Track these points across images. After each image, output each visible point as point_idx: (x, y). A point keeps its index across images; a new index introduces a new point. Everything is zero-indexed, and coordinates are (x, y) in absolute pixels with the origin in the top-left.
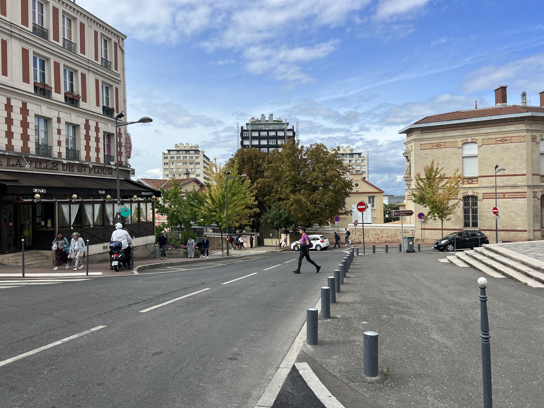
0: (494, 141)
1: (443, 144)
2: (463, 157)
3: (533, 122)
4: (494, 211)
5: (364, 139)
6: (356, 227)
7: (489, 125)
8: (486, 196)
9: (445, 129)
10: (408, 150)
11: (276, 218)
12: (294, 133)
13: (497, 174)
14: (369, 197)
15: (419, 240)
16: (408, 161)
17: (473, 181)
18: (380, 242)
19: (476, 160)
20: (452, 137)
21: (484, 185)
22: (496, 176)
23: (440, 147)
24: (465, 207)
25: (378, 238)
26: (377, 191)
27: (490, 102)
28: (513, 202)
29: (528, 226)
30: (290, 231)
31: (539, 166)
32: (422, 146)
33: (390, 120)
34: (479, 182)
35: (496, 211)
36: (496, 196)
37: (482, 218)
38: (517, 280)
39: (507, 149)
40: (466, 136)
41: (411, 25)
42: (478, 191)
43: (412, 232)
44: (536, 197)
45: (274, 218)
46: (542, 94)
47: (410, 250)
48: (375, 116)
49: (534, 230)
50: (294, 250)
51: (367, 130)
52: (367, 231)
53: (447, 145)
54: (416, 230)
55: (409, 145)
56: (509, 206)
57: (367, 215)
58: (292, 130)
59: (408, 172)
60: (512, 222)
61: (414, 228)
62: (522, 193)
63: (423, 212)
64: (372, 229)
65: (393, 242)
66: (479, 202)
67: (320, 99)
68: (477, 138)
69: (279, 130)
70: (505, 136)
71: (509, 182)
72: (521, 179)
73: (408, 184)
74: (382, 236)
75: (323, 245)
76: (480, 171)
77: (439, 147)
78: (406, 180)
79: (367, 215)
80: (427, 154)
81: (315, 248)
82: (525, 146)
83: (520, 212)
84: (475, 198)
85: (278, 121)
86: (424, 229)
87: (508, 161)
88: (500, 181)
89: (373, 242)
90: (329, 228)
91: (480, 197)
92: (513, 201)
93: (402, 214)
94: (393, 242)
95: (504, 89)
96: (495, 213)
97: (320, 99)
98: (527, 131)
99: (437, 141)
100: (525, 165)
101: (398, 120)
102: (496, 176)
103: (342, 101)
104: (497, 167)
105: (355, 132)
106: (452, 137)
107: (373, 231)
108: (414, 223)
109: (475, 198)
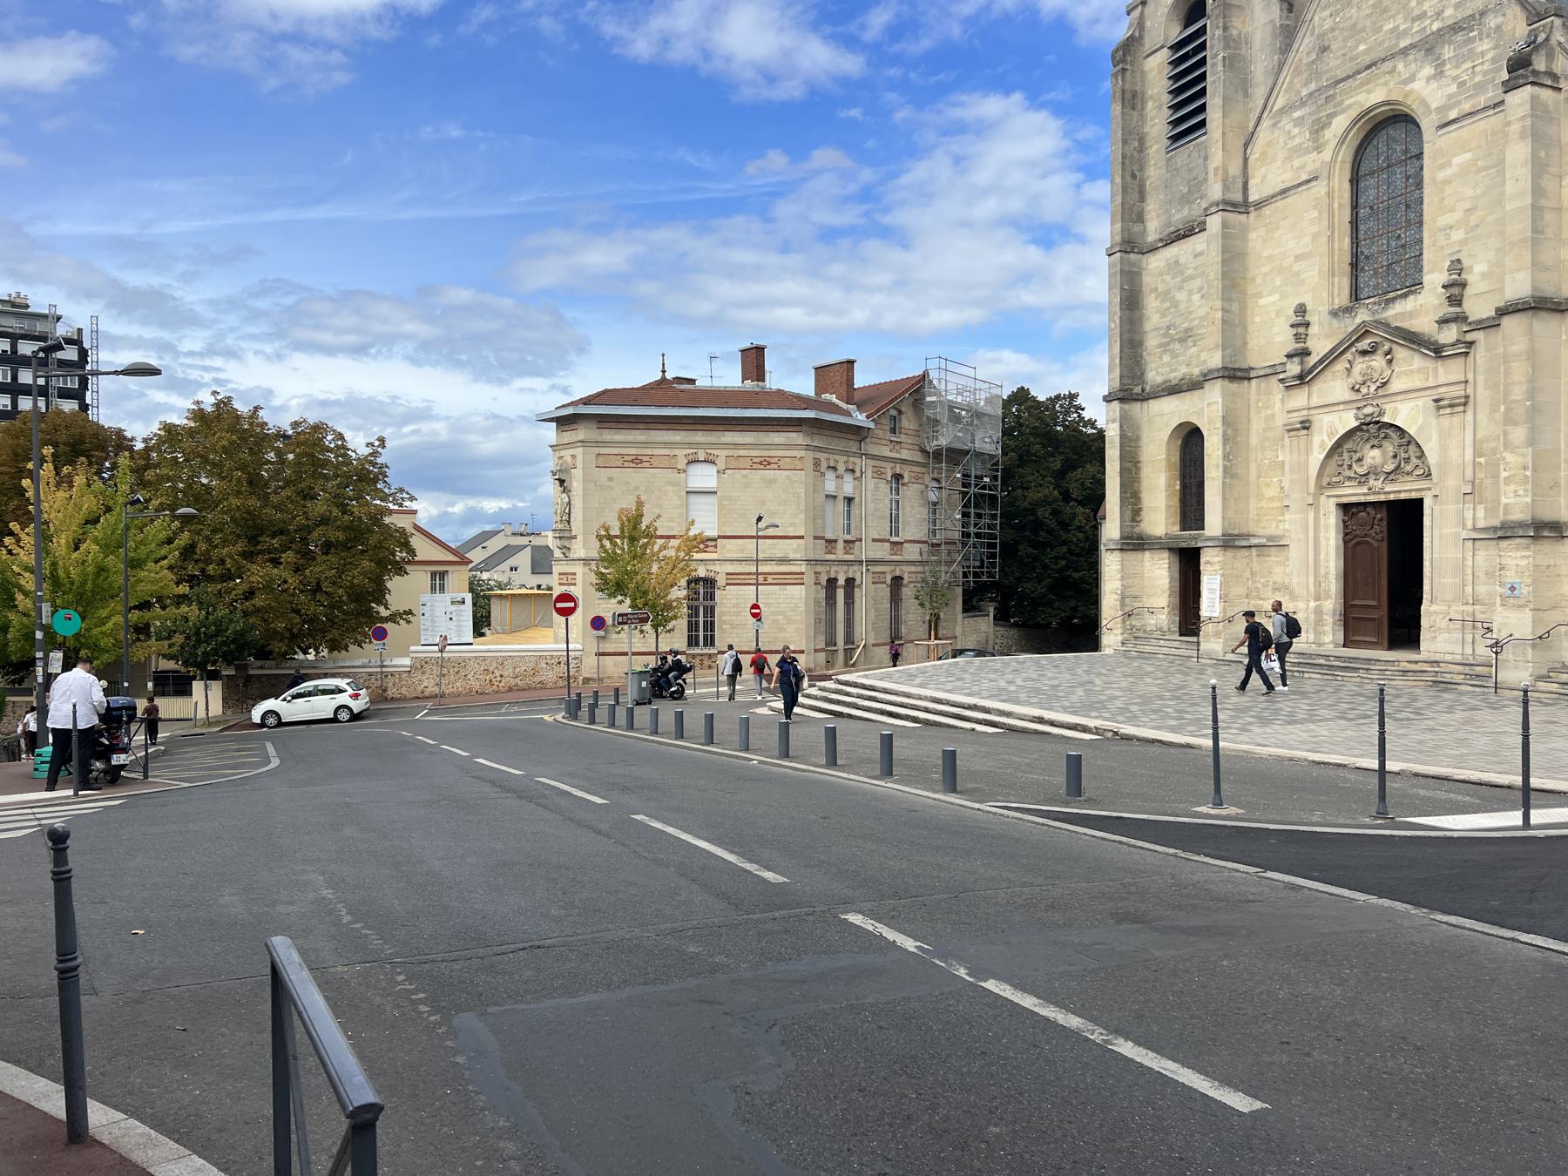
0: (748, 463)
1: (647, 458)
2: (687, 492)
3: (815, 430)
4: (753, 611)
5: (228, 381)
6: (444, 655)
7: (738, 428)
8: (734, 580)
9: (652, 426)
10: (565, 465)
11: (205, 633)
12: (83, 354)
13: (759, 534)
14: (434, 574)
16: (566, 490)
17: (707, 546)
18: (496, 689)
19: (712, 499)
20: (666, 444)
21: (729, 556)
22: (758, 537)
23: (640, 465)
24: (711, 603)
25: (491, 681)
27: (731, 377)
28: (780, 592)
29: (807, 642)
30: (224, 673)
31: (824, 520)
32: (601, 459)
33: (301, 334)
34: (718, 549)
35: (758, 611)
36: (759, 579)
37: (724, 626)
38: (956, 727)
39: (772, 482)
40: (694, 446)
41: (336, 57)
42: (717, 568)
44: (819, 584)
45: (197, 633)
46: (819, 370)
48: (255, 316)
49: (816, 651)
50: (262, 725)
51: (230, 354)
53: (655, 462)
55: (567, 453)
56: (773, 601)
57: (462, 623)
58: (76, 342)
59: (564, 518)
60: (779, 635)
62: (797, 574)
64: (476, 658)
65: (530, 689)
66: (718, 593)
67: (64, 228)
68: (716, 452)
69: (25, 337)
70: (766, 453)
71: (774, 552)
72: (795, 546)
74: (501, 676)
75: (357, 706)
76: (721, 524)
77: (637, 464)
79: (462, 623)
80: (611, 479)
82: (803, 479)
83: (793, 613)
84: (710, 583)
85: (14, 305)
86: (604, 654)
87: (773, 508)
88: (768, 548)
90: (362, 656)
91: (721, 581)
92: (781, 590)
94: (530, 689)
95: (760, 350)
96: (754, 615)
97: (64, 228)
98: (808, 447)
99: (633, 451)
100: (802, 516)
101: (326, 338)
102: (758, 537)
103: (142, 250)
104: (760, 519)
105: (191, 354)
106: (666, 444)
108: (581, 641)
109: (710, 583)
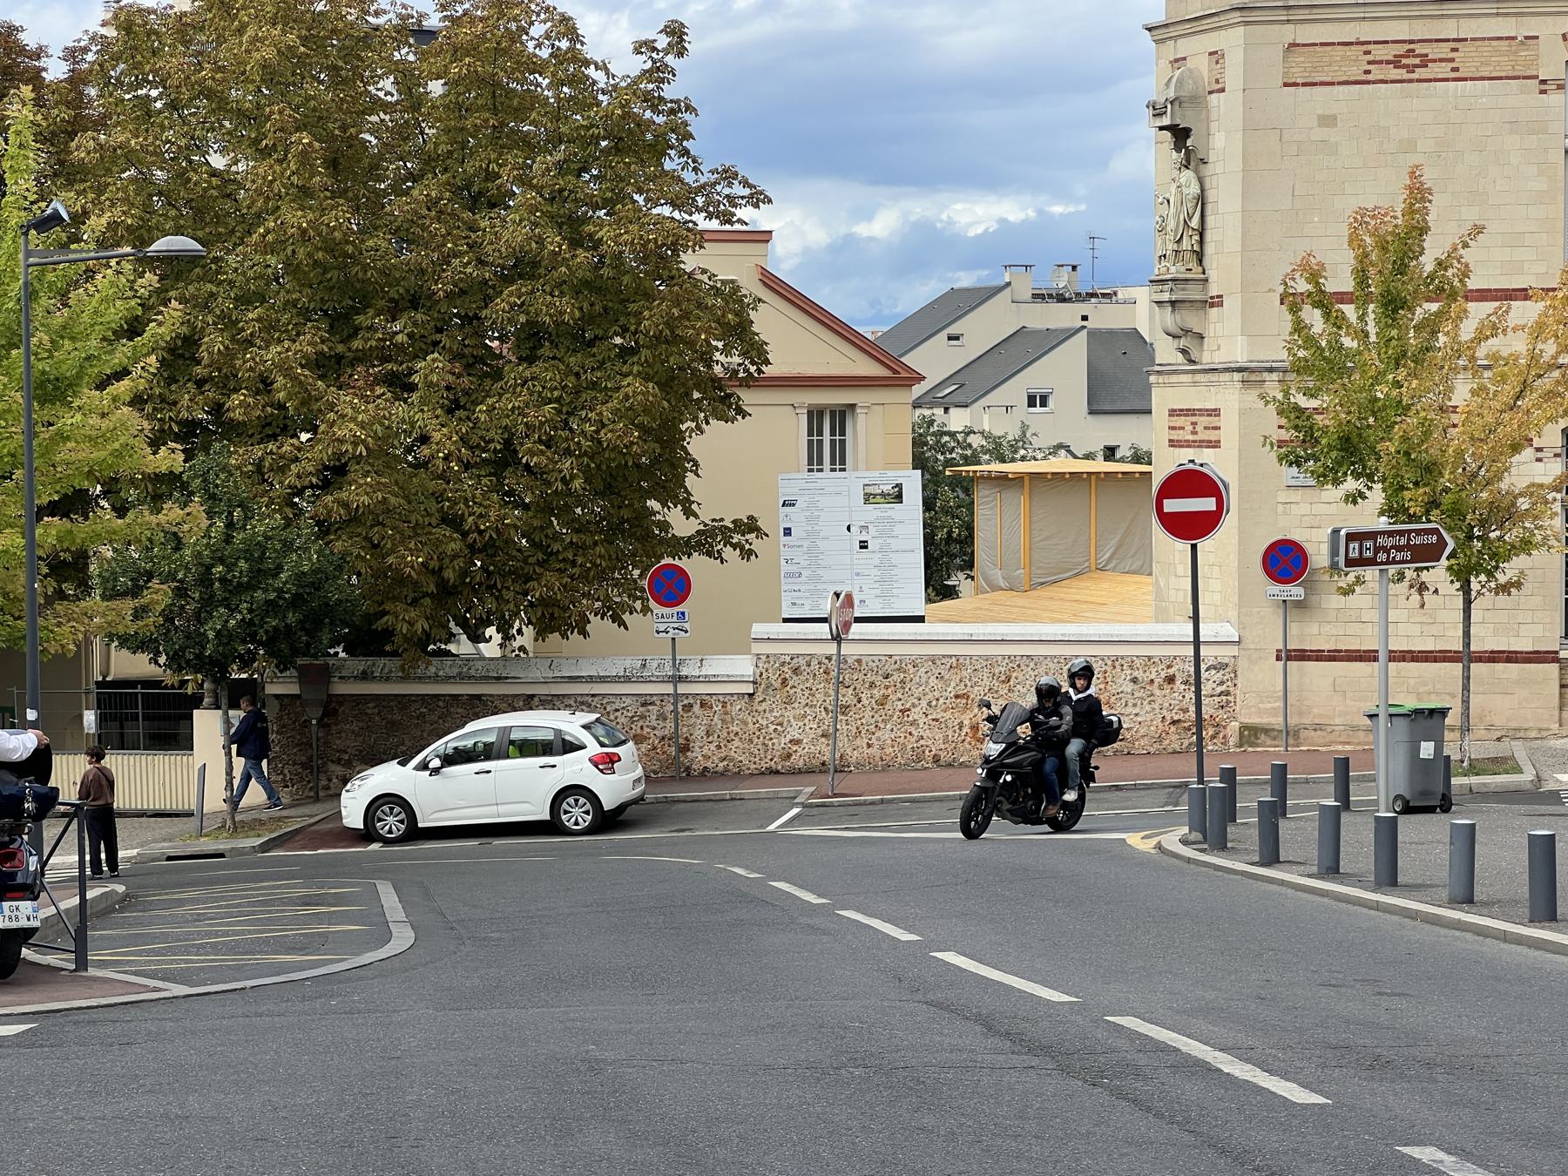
1: (1443, 50)
6: (846, 649)
11: (222, 580)
14: (815, 416)
15: (1266, 731)
23: (1420, 73)
26: (865, 367)
32: (1299, 57)
43: (1218, 676)
45: (205, 580)
47: (1425, 794)
50: (368, 834)
52: (896, 677)
53: (1468, 60)
54: (1242, 665)
55: (1196, 48)
57: (896, 559)
59: (1186, 244)
61: (1234, 651)
63: (1296, 536)
64: (933, 659)
73: (1187, 332)
77: (1411, 69)
78: (1173, 303)
79: (896, 559)
80: (1328, 121)
81: (546, 816)
86: (1302, 656)
89: (936, 759)
93: (1387, 550)
107: (940, 677)
108: (1233, 614)
